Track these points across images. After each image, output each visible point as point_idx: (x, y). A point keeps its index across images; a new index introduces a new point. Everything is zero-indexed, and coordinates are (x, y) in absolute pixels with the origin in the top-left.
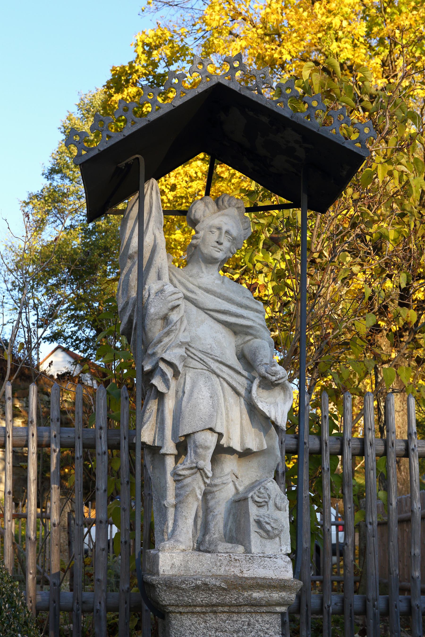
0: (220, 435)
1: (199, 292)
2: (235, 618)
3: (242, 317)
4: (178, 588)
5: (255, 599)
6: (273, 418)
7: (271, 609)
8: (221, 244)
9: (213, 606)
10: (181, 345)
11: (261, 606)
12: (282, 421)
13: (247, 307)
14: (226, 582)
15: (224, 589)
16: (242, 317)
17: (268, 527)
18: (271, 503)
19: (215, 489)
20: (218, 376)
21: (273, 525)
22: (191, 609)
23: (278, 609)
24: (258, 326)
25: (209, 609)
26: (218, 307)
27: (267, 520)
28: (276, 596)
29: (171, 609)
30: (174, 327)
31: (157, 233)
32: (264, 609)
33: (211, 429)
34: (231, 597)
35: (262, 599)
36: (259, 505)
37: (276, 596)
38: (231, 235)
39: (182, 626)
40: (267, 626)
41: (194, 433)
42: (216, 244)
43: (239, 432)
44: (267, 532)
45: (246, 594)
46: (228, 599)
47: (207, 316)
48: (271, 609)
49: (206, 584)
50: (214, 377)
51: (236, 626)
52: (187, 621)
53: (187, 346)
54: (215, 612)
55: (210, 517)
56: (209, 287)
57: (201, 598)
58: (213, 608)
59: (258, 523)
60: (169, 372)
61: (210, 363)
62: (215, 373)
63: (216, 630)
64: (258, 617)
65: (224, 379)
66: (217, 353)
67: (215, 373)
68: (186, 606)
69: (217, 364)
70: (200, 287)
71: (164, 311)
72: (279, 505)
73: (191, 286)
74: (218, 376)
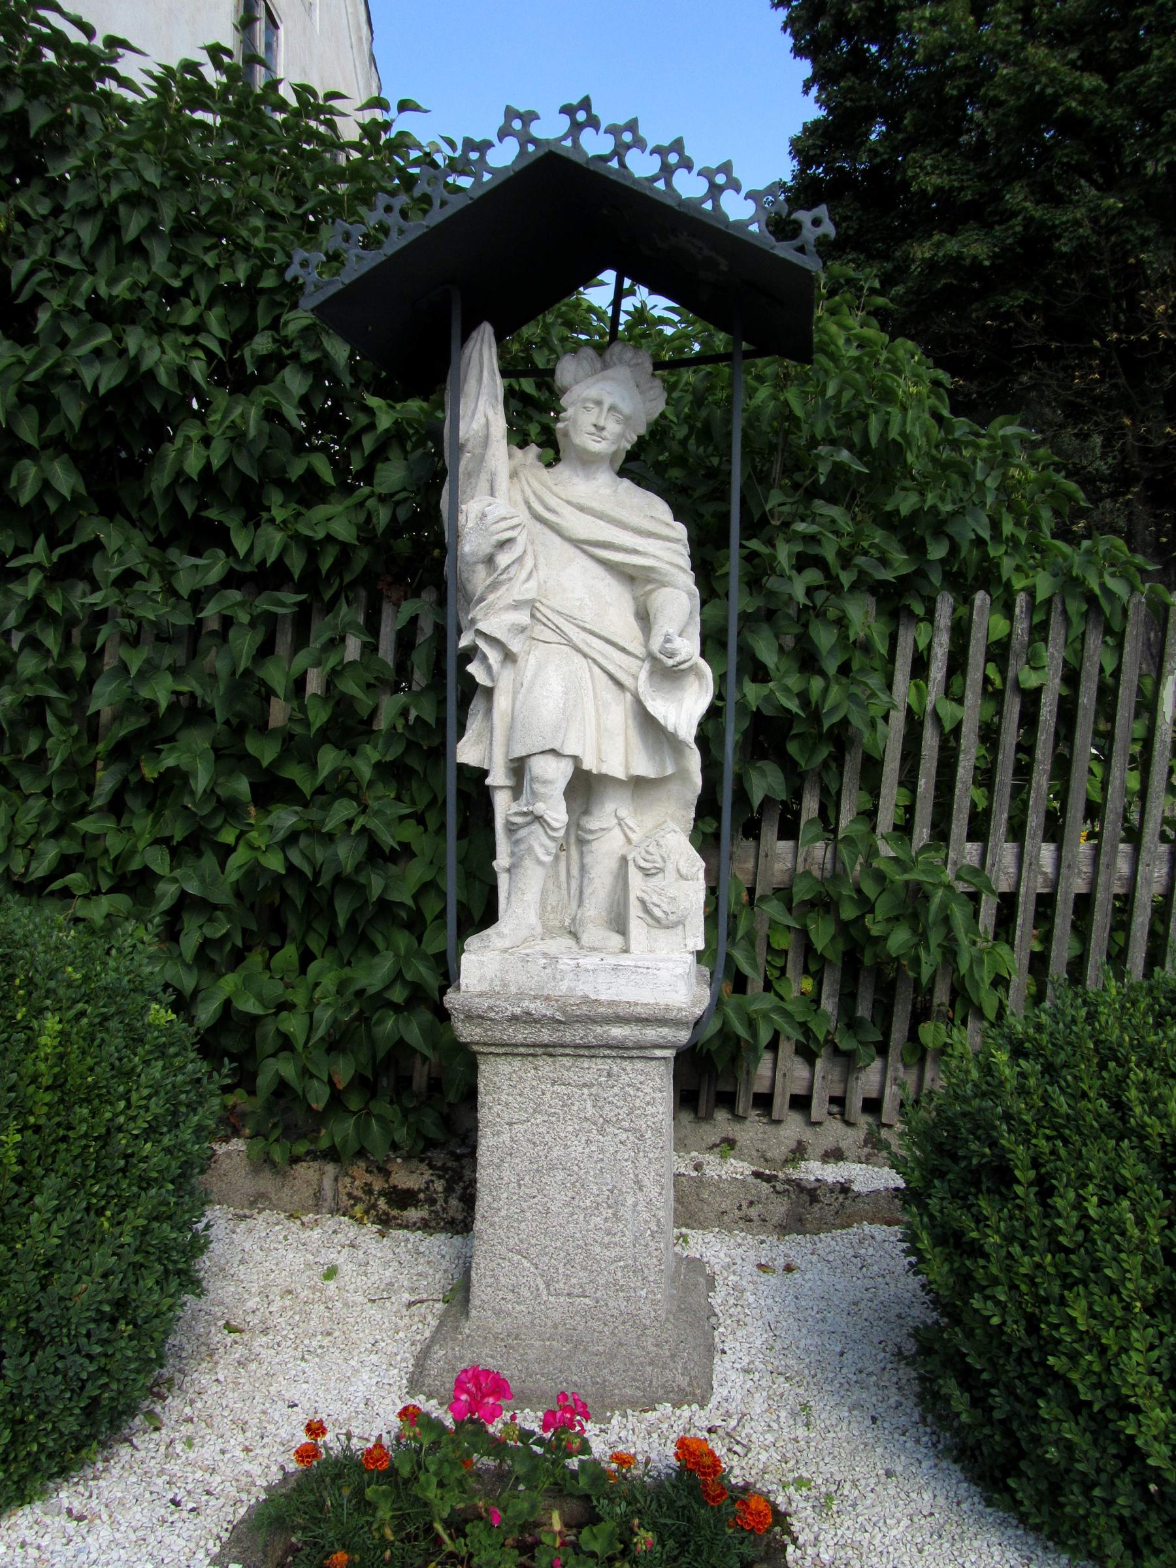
0: (576, 759)
1: (567, 510)
2: (586, 1065)
3: (635, 552)
4: (482, 1017)
5: (614, 1038)
6: (670, 728)
7: (647, 1053)
8: (603, 429)
9: (546, 1046)
10: (517, 605)
11: (627, 1048)
12: (687, 730)
13: (650, 535)
14: (564, 1012)
15: (560, 1022)
16: (635, 552)
17: (657, 912)
18: (670, 867)
19: (590, 837)
20: (585, 656)
21: (665, 907)
22: (510, 1050)
23: (659, 1053)
24: (667, 567)
25: (539, 1051)
26: (600, 537)
27: (655, 899)
28: (651, 1034)
29: (476, 1048)
30: (504, 576)
31: (491, 414)
32: (634, 1053)
33: (553, 751)
34: (571, 1035)
35: (625, 1037)
36: (647, 873)
37: (651, 1034)
38: (620, 413)
39: (497, 1074)
40: (642, 1078)
41: (529, 756)
42: (593, 430)
43: (616, 753)
44: (657, 920)
45: (599, 1030)
46: (568, 1038)
47: (578, 552)
48: (647, 1053)
49: (529, 1014)
50: (578, 659)
51: (588, 1078)
52: (505, 1067)
53: (531, 605)
54: (551, 1055)
55: (586, 881)
56: (582, 501)
57: (522, 1034)
58: (549, 1050)
59: (642, 902)
60: (493, 656)
61: (571, 634)
62: (579, 650)
63: (554, 1083)
64: (626, 1063)
65: (594, 661)
66: (588, 618)
67: (579, 650)
68: (503, 1046)
69: (584, 635)
70: (568, 502)
71: (486, 549)
72: (684, 871)
73: (553, 502)
74: (585, 656)
